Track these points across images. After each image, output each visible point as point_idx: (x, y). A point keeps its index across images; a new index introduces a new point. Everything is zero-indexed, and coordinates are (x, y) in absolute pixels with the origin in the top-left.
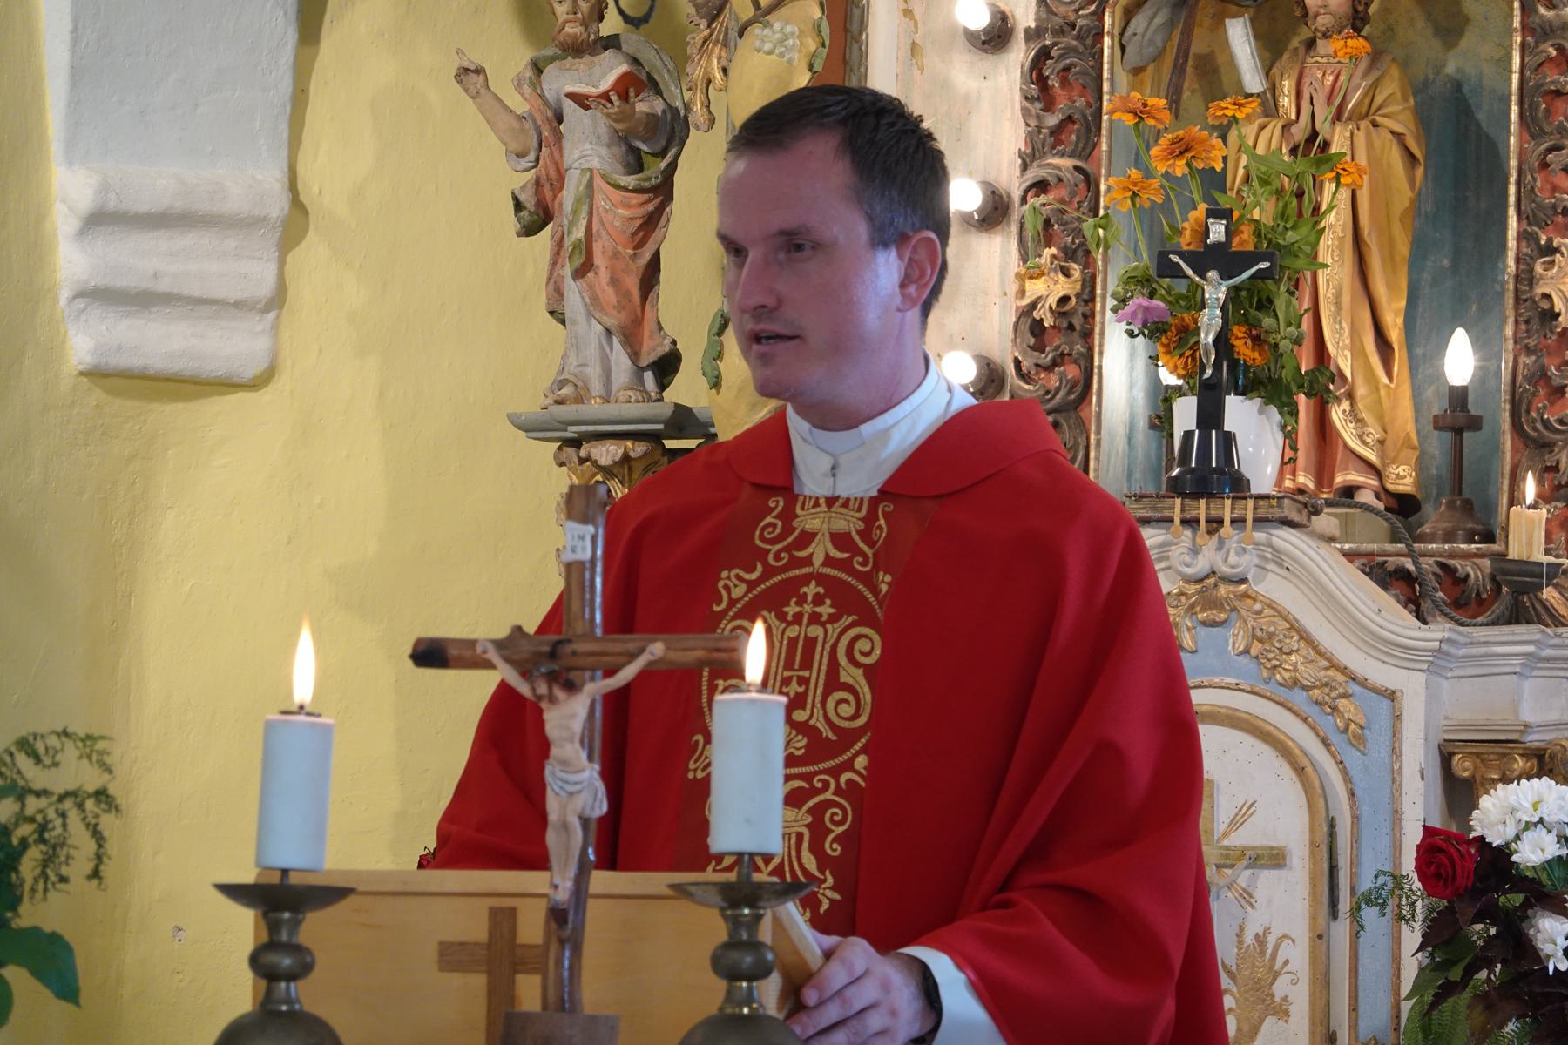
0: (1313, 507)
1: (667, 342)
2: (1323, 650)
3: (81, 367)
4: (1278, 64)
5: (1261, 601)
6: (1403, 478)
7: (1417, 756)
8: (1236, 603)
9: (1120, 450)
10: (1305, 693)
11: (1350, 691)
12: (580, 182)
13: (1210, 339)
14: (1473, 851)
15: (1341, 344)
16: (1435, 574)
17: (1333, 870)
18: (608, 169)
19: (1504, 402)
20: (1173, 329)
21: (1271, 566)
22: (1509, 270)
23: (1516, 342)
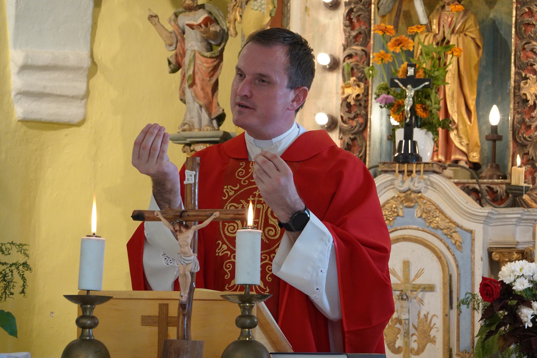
1: (221, 110)
2: (447, 216)
3: (19, 119)
4: (432, 14)
5: (426, 200)
6: (475, 157)
11: (457, 230)
13: (409, 109)
14: (499, 285)
15: (454, 111)
16: (486, 190)
19: (510, 130)
21: (429, 187)
22: (512, 85)
23: (514, 110)
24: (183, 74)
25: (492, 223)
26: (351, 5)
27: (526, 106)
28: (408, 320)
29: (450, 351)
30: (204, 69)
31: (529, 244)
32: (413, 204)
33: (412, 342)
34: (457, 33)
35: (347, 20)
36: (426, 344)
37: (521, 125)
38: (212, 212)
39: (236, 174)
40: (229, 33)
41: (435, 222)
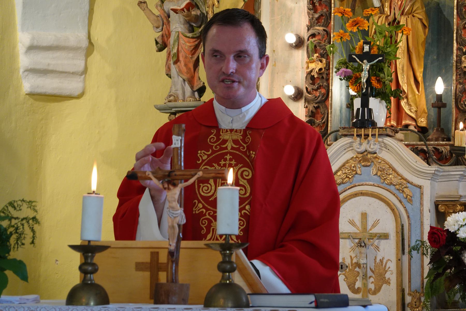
1: (202, 83)
3: (26, 92)
5: (381, 159)
6: (423, 122)
7: (428, 205)
8: (373, 160)
9: (338, 114)
11: (408, 186)
12: (175, 35)
13: (365, 81)
14: (445, 234)
15: (404, 82)
16: (433, 151)
17: (403, 240)
18: (183, 31)
19: (453, 99)
20: (353, 78)
21: (384, 149)
23: (456, 81)
24: (169, 52)
25: (438, 179)
28: (366, 264)
29: (403, 291)
30: (186, 48)
33: (370, 284)
35: (311, 5)
37: (462, 94)
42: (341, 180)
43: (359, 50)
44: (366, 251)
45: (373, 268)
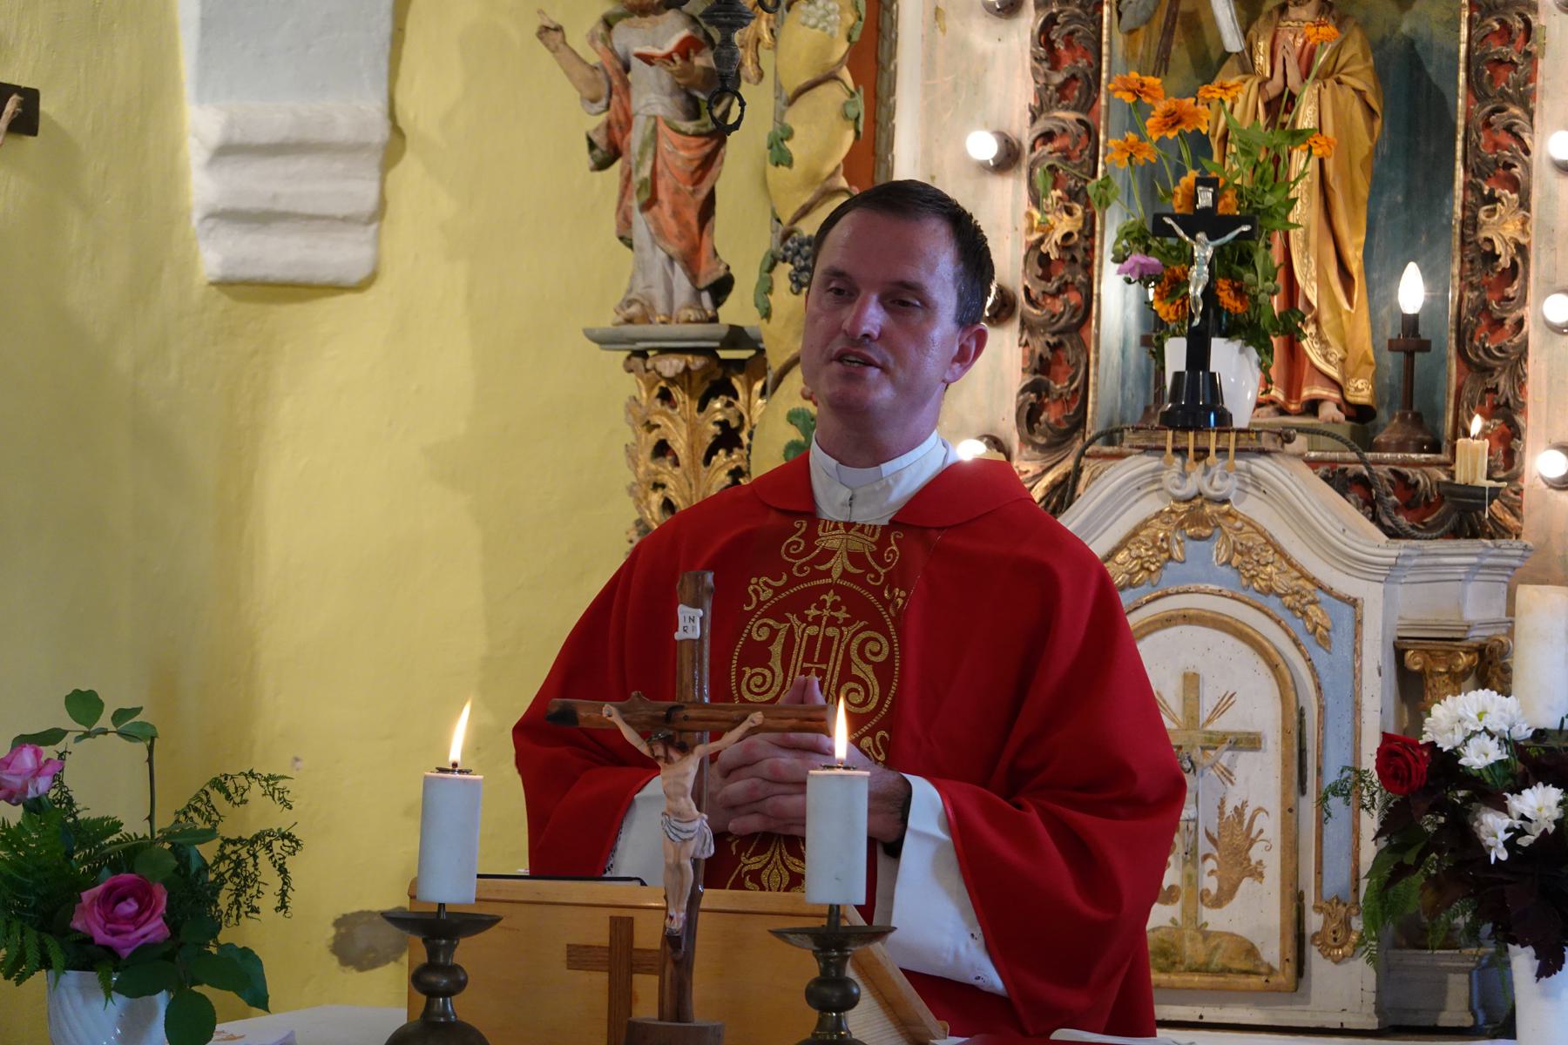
0: (1286, 435)
1: (722, 267)
2: (1294, 562)
3: (211, 279)
4: (1254, 26)
5: (1241, 520)
6: (1361, 391)
8: (1220, 521)
9: (1115, 364)
10: (1278, 600)
11: (1318, 599)
12: (646, 127)
13: (1199, 293)
14: (1426, 754)
15: (1308, 276)
16: (1389, 480)
17: (1302, 752)
19: (1451, 330)
20: (1166, 279)
21: (1250, 489)
22: (1456, 216)
23: (1461, 279)
24: (626, 172)
25: (1405, 576)
26: (1052, 7)
27: (1493, 270)
28: (1195, 820)
29: (1300, 897)
30: (679, 163)
31: (1497, 627)
32: (1208, 532)
33: (1205, 876)
34: (1317, 77)
35: (1041, 46)
36: (1240, 881)
37: (1478, 319)
38: (746, 712)
39: (783, 548)
40: (743, 73)
41: (1263, 576)
42: (1127, 576)
43: (1183, 201)
44: (1195, 784)
45: (1214, 832)
